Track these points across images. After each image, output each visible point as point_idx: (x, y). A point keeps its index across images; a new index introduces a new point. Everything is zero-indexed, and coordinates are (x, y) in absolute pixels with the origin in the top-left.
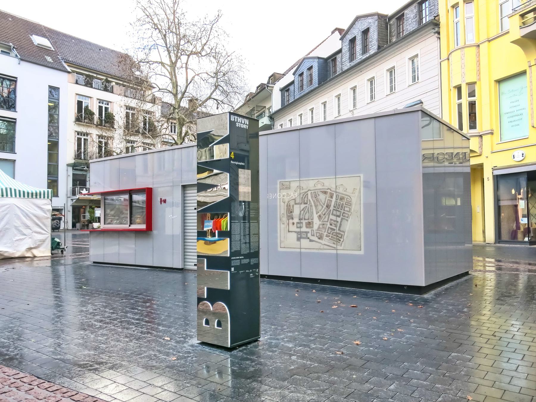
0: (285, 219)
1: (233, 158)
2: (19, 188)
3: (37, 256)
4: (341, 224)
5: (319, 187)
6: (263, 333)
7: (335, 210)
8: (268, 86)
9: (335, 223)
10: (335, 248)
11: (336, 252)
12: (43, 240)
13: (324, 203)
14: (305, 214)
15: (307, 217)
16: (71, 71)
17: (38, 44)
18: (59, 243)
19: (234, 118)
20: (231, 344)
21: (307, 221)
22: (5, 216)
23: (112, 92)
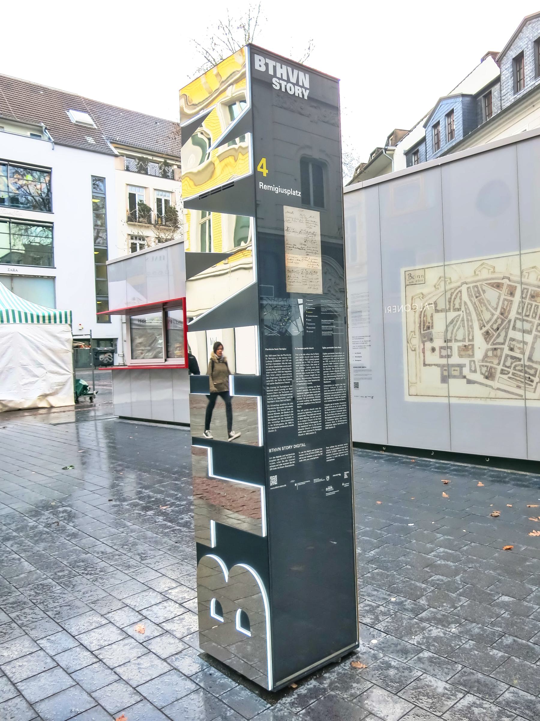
0: (416, 341)
1: (265, 175)
2: (38, 311)
3: (54, 406)
4: (533, 348)
5: (485, 274)
6: (367, 620)
7: (519, 319)
8: (386, 150)
9: (521, 345)
10: (522, 396)
11: (524, 405)
12: (62, 382)
13: (495, 306)
14: (457, 331)
15: (460, 337)
16: (118, 154)
17: (76, 122)
18: (85, 387)
19: (267, 65)
20: (275, 680)
21: (460, 344)
22: (6, 350)
23: (173, 179)
